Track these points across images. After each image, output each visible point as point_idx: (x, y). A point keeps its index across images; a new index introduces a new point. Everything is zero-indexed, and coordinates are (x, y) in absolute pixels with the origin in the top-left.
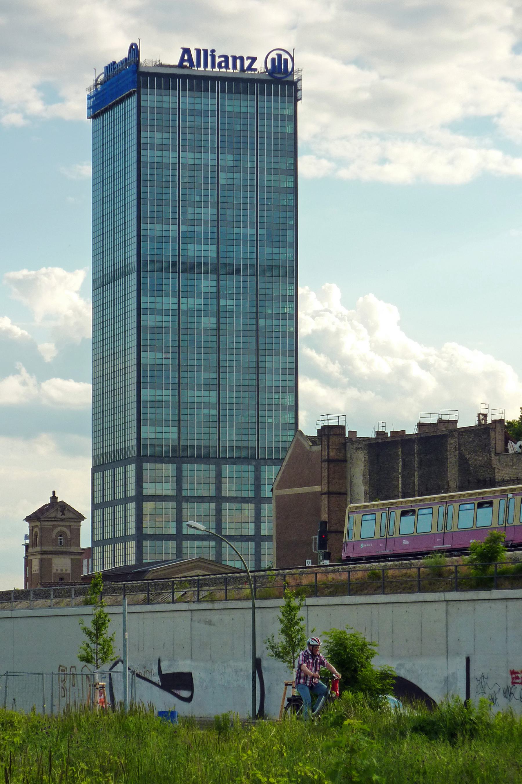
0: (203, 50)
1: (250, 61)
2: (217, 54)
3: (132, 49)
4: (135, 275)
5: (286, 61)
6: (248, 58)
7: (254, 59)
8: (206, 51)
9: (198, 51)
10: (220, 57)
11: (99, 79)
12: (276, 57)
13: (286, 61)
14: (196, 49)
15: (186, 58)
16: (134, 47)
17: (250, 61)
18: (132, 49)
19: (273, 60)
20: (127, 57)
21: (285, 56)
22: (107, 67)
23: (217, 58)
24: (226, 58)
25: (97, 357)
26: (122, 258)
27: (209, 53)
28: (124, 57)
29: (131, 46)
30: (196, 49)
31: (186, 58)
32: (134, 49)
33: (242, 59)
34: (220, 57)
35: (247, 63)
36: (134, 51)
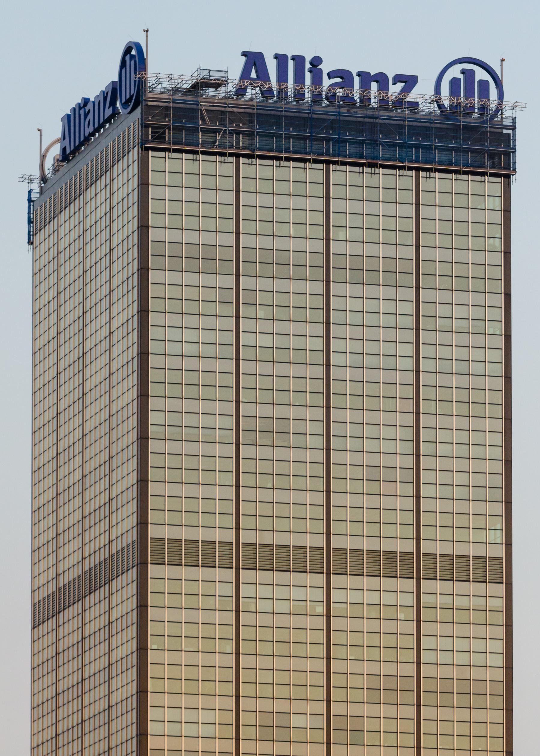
0: (294, 58)
1: (400, 85)
2: (326, 68)
3: (128, 58)
4: (133, 574)
5: (484, 85)
6: (398, 78)
7: (409, 82)
8: (299, 60)
9: (281, 59)
10: (330, 76)
11: (47, 172)
13: (484, 85)
14: (276, 57)
15: (253, 75)
16: (133, 52)
17: (400, 85)
18: (128, 58)
19: (454, 83)
20: (116, 79)
21: (481, 74)
22: (68, 116)
23: (325, 77)
24: (344, 76)
25: (42, 697)
26: (104, 540)
27: (308, 66)
28: (109, 82)
29: (128, 50)
30: (276, 57)
31: (253, 75)
32: (132, 57)
33: (381, 79)
34: (330, 76)
35: (395, 89)
36: (134, 58)
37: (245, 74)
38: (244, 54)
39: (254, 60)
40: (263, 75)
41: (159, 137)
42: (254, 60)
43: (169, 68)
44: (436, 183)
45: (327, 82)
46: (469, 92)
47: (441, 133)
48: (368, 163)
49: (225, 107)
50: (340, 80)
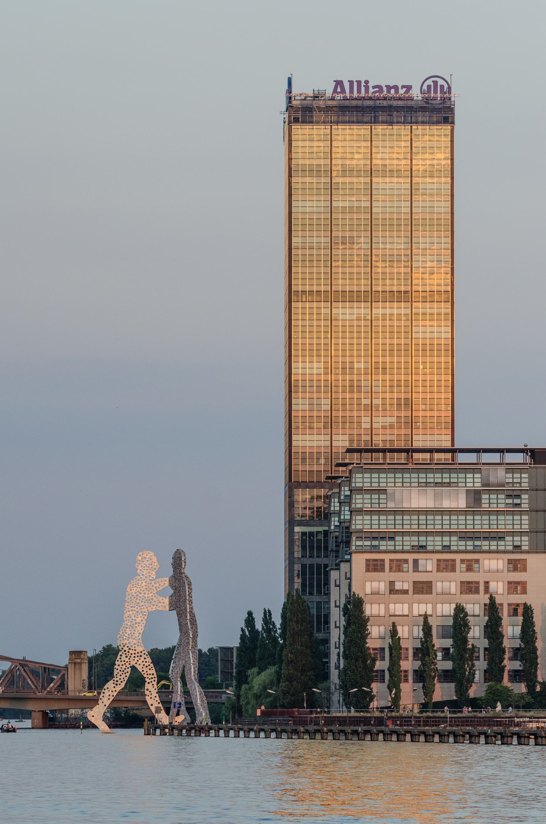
1: (405, 89)
2: (370, 85)
6: (403, 87)
8: (359, 82)
9: (351, 82)
10: (374, 87)
12: (432, 84)
13: (442, 87)
15: (339, 90)
17: (405, 89)
19: (429, 87)
21: (440, 82)
24: (380, 87)
31: (339, 90)
33: (396, 88)
35: (402, 91)
37: (335, 91)
38: (334, 81)
39: (339, 83)
40: (343, 91)
41: (296, 120)
42: (339, 83)
43: (303, 88)
44: (419, 129)
45: (371, 90)
46: (436, 92)
47: (423, 109)
48: (324, 531)
49: (316, 820)
50: (378, 89)
